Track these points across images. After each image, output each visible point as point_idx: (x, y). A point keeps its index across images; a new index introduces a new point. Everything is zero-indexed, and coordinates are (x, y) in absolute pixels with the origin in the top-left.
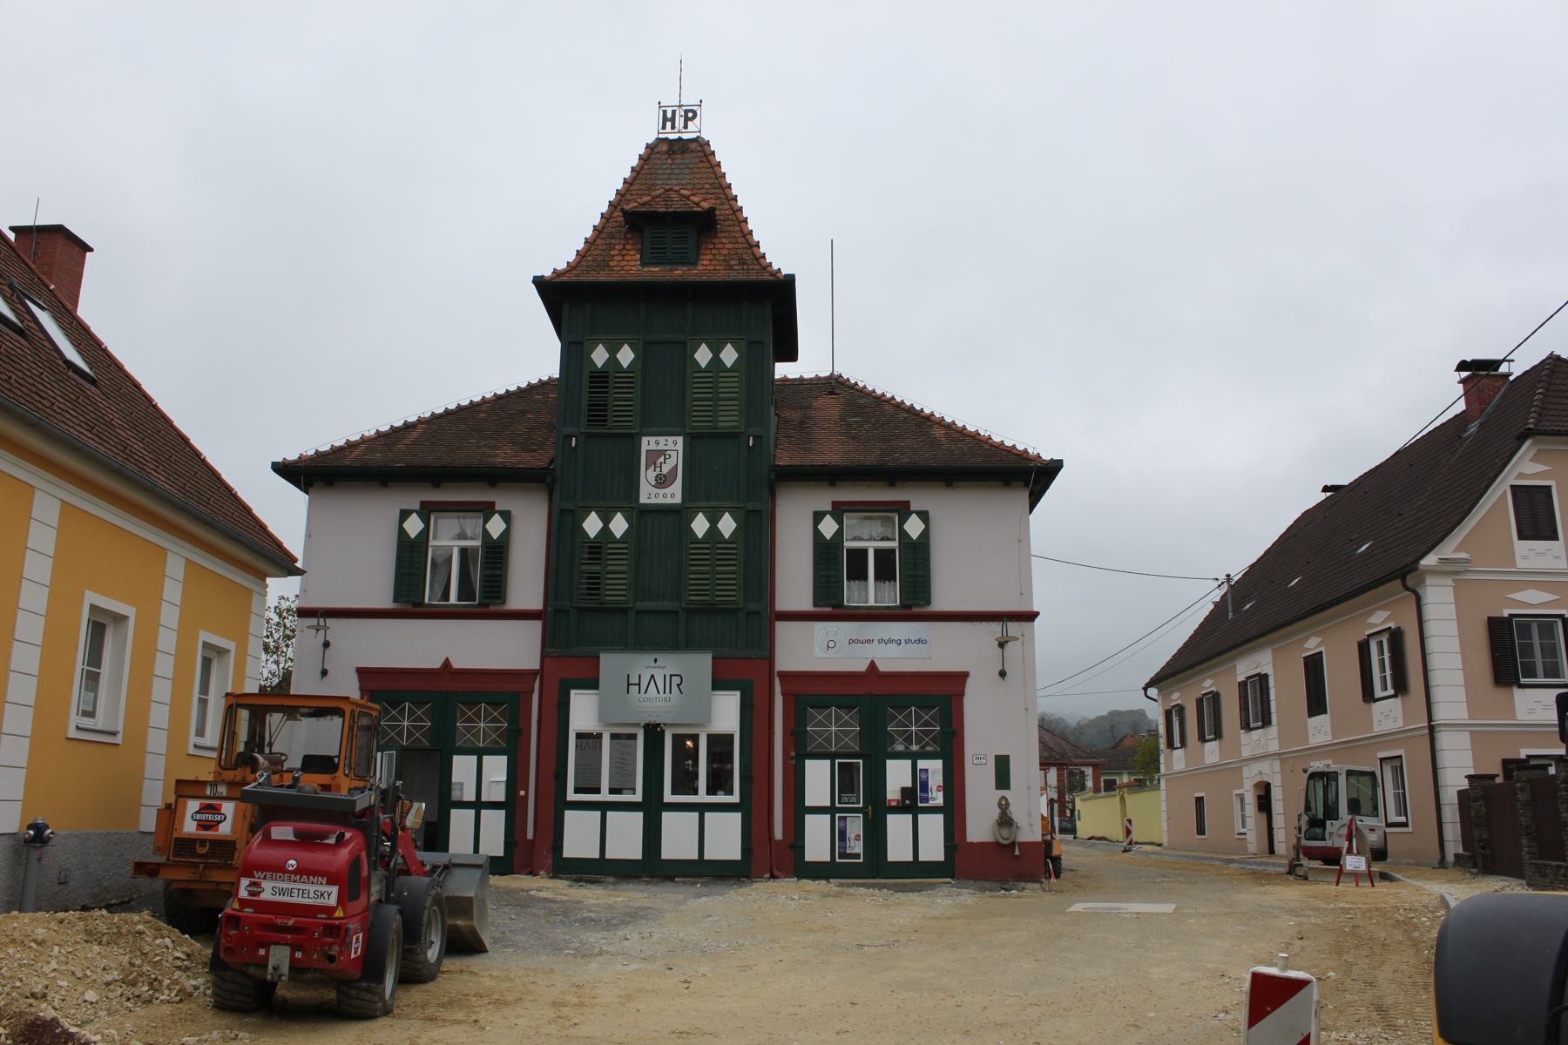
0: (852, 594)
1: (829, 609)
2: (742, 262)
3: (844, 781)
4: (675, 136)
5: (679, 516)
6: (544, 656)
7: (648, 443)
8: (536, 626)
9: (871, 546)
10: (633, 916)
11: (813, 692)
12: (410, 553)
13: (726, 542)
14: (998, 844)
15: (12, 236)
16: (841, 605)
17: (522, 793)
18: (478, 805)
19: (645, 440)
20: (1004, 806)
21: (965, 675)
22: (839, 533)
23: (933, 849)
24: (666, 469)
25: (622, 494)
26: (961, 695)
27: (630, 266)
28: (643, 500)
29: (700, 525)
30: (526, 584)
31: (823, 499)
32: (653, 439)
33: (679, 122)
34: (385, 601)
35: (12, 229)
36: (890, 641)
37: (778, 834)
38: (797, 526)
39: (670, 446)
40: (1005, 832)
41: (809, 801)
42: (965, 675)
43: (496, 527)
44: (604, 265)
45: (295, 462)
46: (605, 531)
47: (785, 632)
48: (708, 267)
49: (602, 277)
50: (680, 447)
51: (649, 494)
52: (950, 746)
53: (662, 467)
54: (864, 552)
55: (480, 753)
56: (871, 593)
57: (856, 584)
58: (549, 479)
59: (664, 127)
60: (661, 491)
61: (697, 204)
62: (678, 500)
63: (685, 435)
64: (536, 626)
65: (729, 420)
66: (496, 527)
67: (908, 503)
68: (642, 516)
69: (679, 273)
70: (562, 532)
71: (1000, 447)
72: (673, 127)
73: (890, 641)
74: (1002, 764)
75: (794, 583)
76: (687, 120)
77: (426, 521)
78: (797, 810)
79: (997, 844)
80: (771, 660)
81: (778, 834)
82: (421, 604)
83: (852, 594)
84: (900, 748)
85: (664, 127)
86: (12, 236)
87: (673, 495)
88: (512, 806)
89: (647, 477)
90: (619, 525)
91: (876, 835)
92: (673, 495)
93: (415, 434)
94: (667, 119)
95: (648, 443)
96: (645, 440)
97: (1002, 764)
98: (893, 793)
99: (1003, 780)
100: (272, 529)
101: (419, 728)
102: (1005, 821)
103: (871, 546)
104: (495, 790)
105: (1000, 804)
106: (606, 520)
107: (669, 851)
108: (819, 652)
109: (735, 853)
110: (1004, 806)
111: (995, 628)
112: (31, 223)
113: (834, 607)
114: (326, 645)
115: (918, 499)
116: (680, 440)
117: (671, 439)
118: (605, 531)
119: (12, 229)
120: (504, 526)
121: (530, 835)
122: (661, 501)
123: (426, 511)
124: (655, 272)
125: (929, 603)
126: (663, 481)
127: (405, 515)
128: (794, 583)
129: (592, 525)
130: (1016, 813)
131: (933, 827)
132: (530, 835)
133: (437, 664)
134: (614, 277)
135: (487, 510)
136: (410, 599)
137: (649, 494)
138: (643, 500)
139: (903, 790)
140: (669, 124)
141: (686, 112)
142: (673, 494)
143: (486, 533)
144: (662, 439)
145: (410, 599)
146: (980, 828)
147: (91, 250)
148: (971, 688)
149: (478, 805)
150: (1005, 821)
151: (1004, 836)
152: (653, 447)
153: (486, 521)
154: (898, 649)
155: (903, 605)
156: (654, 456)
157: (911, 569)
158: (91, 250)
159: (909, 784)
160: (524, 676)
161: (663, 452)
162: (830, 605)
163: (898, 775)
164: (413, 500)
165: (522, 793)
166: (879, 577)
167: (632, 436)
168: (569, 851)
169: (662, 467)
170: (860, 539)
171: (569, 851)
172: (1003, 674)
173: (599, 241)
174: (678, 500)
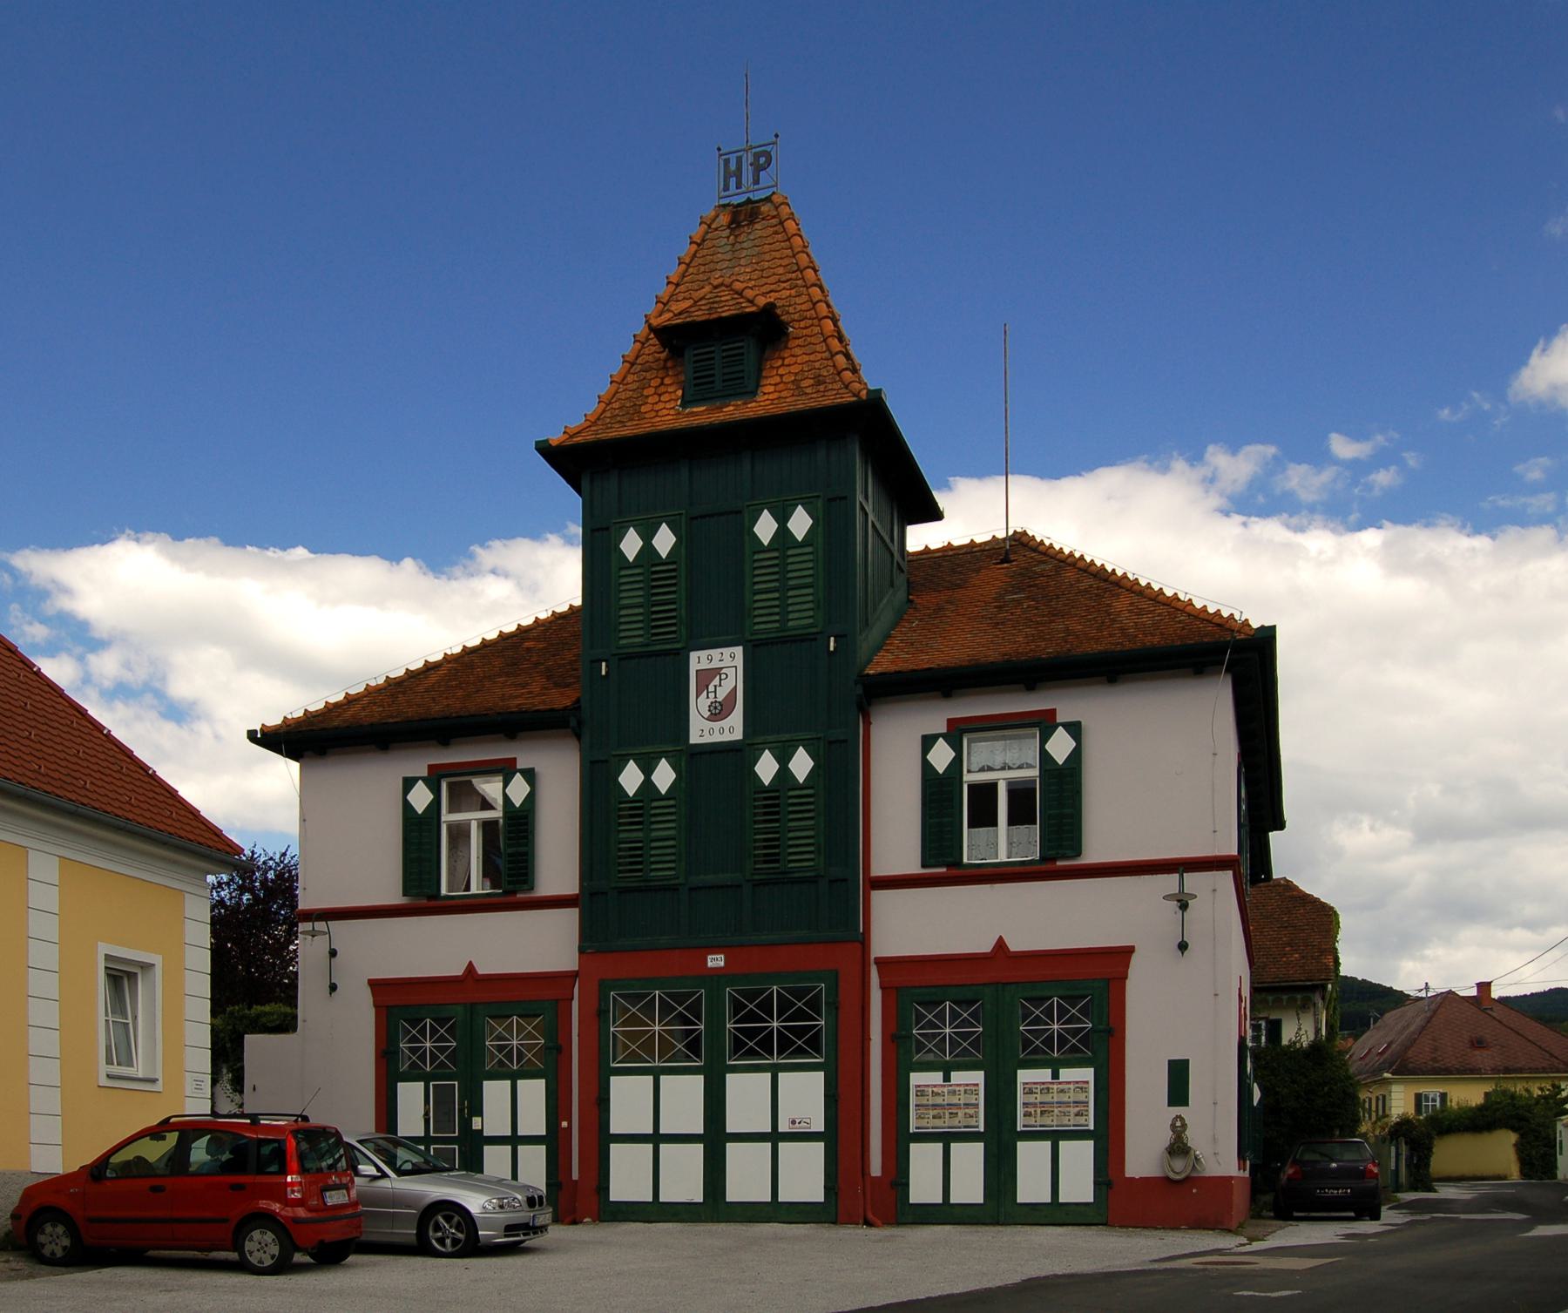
0: (975, 846)
1: (944, 870)
2: (819, 381)
3: (439, 1107)
4: (742, 199)
5: (738, 755)
7: (698, 660)
8: (571, 916)
9: (1002, 780)
10: (375, 1264)
11: (926, 983)
12: (419, 833)
13: (663, 798)
14: (1167, 1179)
16: (958, 863)
18: (514, 1140)
19: (693, 656)
20: (1179, 1128)
21: (1129, 951)
22: (957, 763)
23: (1079, 1186)
24: (722, 694)
25: (662, 729)
27: (668, 411)
28: (694, 739)
29: (766, 768)
30: (558, 863)
31: (934, 717)
32: (703, 654)
33: (747, 172)
34: (393, 895)
37: (876, 1169)
38: (899, 755)
39: (727, 662)
40: (1179, 1164)
42: (1129, 951)
43: (1060, 746)
44: (635, 412)
45: (280, 726)
46: (648, 785)
48: (774, 395)
49: (627, 431)
50: (739, 661)
51: (702, 731)
52: (1102, 1045)
53: (716, 692)
54: (993, 787)
55: (514, 1077)
56: (1003, 842)
57: (983, 831)
58: (573, 722)
59: (726, 188)
60: (716, 725)
61: (751, 302)
62: (738, 735)
64: (571, 916)
65: (801, 617)
66: (1060, 746)
67: (1053, 712)
68: (693, 760)
69: (733, 411)
71: (1202, 617)
74: (1178, 1075)
76: (758, 169)
77: (957, 747)
78: (899, 1140)
79: (1167, 1180)
80: (864, 942)
81: (876, 1169)
82: (436, 895)
83: (975, 846)
85: (726, 188)
87: (732, 729)
88: (554, 1140)
89: (699, 706)
90: (664, 776)
91: (1000, 1170)
92: (732, 729)
93: (434, 677)
94: (732, 174)
95: (698, 660)
96: (693, 656)
97: (1178, 1075)
99: (1178, 1090)
101: (442, 1050)
102: (1178, 1148)
103: (1002, 780)
104: (534, 1121)
105: (1173, 1126)
106: (648, 770)
107: (736, 1191)
109: (977, 1197)
110: (1179, 1128)
111: (1169, 882)
113: (948, 866)
114: (333, 953)
115: (1067, 705)
117: (727, 651)
118: (648, 785)
120: (431, 797)
122: (717, 738)
123: (956, 733)
124: (702, 415)
125: (1079, 854)
126: (719, 712)
127: (409, 784)
128: (895, 838)
129: (630, 778)
130: (1193, 1137)
131: (1079, 1158)
132: (575, 1176)
133: (458, 971)
134: (645, 428)
135: (1045, 723)
136: (423, 894)
137: (702, 731)
138: (694, 739)
140: (733, 181)
141: (757, 156)
142: (732, 728)
143: (1045, 757)
144: (715, 653)
145: (423, 894)
146: (1143, 1156)
149: (514, 1140)
150: (1178, 1148)
151: (1179, 1166)
152: (705, 665)
153: (1044, 740)
155: (1043, 859)
156: (706, 677)
157: (1055, 804)
160: (570, 977)
161: (717, 671)
162: (943, 863)
164: (418, 766)
165: (564, 1124)
166: (1013, 821)
167: (676, 652)
169: (716, 692)
170: (990, 769)
171: (916, 1196)
172: (1183, 946)
173: (630, 378)
174: (738, 735)
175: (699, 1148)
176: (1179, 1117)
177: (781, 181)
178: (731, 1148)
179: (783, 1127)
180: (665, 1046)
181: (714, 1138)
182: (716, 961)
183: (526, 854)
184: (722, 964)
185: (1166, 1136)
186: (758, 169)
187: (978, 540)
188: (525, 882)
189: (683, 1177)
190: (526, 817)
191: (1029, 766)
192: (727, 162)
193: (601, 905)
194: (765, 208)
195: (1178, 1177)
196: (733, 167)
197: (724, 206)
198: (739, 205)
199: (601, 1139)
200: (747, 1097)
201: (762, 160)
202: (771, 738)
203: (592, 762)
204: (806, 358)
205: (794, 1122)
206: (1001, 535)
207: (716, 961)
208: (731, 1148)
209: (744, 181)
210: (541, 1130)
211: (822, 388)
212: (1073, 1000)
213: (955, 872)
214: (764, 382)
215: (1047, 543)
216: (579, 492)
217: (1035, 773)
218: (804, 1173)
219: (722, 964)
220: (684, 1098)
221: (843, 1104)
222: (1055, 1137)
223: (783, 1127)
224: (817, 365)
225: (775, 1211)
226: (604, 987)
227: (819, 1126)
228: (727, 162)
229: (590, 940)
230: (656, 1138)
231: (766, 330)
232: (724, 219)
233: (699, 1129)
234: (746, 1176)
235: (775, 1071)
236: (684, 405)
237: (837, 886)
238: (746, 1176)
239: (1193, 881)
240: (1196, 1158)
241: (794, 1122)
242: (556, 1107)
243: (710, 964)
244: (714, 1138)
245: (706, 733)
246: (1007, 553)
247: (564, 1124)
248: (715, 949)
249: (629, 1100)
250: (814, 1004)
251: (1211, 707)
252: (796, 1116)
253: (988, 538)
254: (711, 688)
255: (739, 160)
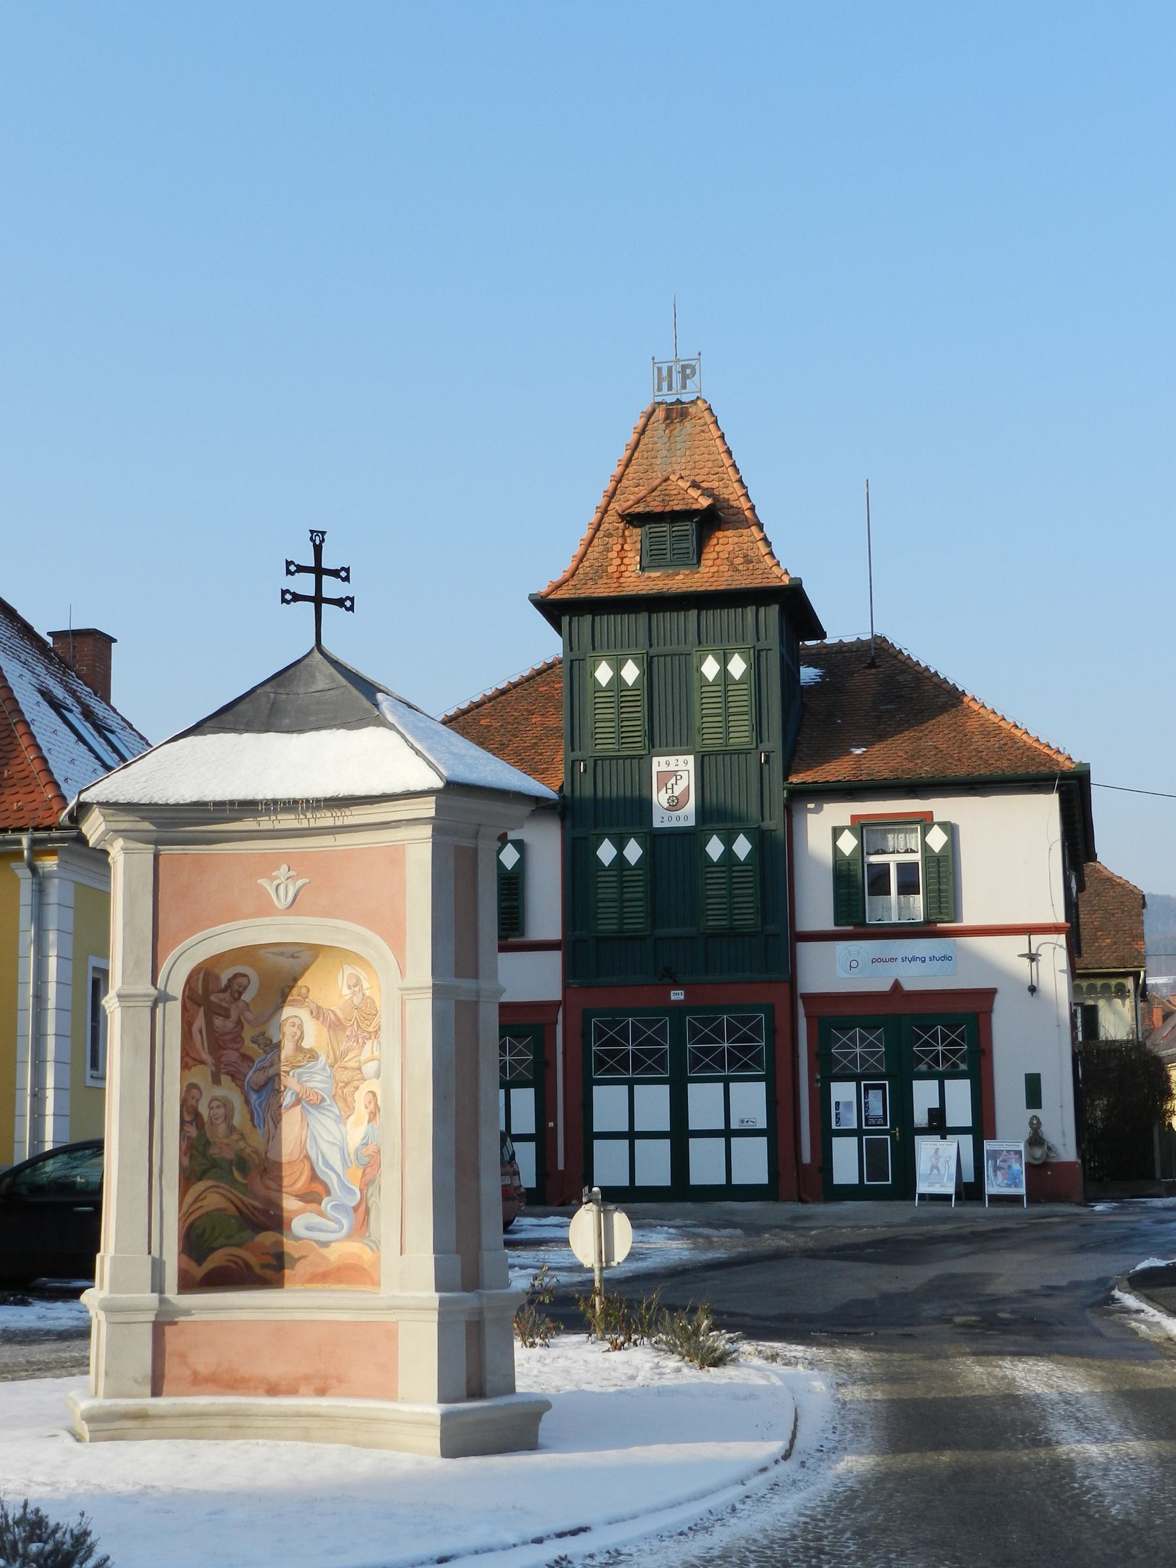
1: (850, 928)
4: (671, 399)
5: (690, 839)
6: (565, 987)
7: (659, 764)
11: (840, 1013)
15: (50, 640)
16: (863, 923)
17: (551, 1124)
19: (655, 760)
20: (1035, 1125)
26: (989, 1012)
28: (657, 824)
29: (715, 848)
30: (545, 914)
32: (663, 759)
35: (49, 634)
36: (914, 959)
37: (806, 1157)
39: (681, 766)
40: (1038, 1152)
41: (532, 1145)
47: (808, 953)
48: (716, 568)
51: (660, 820)
52: (978, 1070)
59: (660, 389)
62: (691, 822)
63: (696, 753)
66: (937, 839)
70: (577, 860)
72: (670, 388)
73: (914, 959)
74: (1033, 1084)
75: (816, 906)
76: (685, 377)
78: (825, 1135)
80: (792, 981)
81: (806, 1157)
84: (923, 1067)
85: (660, 389)
86: (50, 640)
88: (542, 1137)
90: (633, 852)
94: (663, 378)
95: (659, 764)
96: (655, 760)
97: (1033, 1084)
98: (920, 1118)
99: (1034, 1096)
100: (342, 732)
103: (892, 860)
105: (1031, 1123)
108: (841, 973)
110: (1035, 1125)
112: (67, 628)
113: (855, 925)
115: (942, 808)
116: (691, 759)
117: (681, 758)
119: (49, 634)
121: (561, 1167)
122: (674, 824)
129: (606, 852)
132: (561, 1167)
135: (925, 821)
139: (931, 1111)
140: (665, 385)
141: (684, 368)
143: (926, 847)
144: (672, 759)
147: (115, 641)
148: (999, 1004)
150: (1036, 1140)
152: (664, 768)
153: (924, 834)
154: (916, 968)
156: (666, 776)
158: (115, 641)
159: (936, 1105)
163: (924, 1094)
167: (641, 757)
168: (837, 1180)
171: (837, 1180)
174: (691, 822)
175: (667, 1143)
176: (1035, 1117)
177: (708, 386)
178: (693, 1143)
179: (734, 1125)
180: (638, 1063)
181: (680, 1134)
182: (677, 995)
183: (517, 907)
184: (682, 997)
185: (1027, 1132)
186: (685, 377)
187: (846, 640)
188: (517, 929)
189: (655, 1167)
190: (516, 878)
191: (912, 851)
192: (660, 369)
193: (580, 949)
194: (692, 410)
195: (1037, 1163)
196: (665, 373)
197: (659, 403)
198: (671, 404)
199: (584, 1135)
200: (705, 1102)
201: (688, 371)
202: (720, 826)
203: (574, 839)
204: (736, 540)
205: (742, 1121)
206: (867, 637)
207: (677, 995)
208: (693, 1143)
209: (674, 385)
210: (531, 1129)
211: (751, 566)
212: (952, 1028)
213: (861, 930)
214: (706, 550)
215: (906, 653)
216: (560, 634)
217: (917, 857)
218: (752, 1163)
219: (682, 997)
220: (653, 1104)
221: (780, 1105)
222: (665, 656)
223: (734, 1125)
224: (745, 546)
225: (730, 1191)
226: (587, 1015)
227: (762, 1124)
228: (660, 369)
229: (570, 971)
230: (632, 1135)
231: (712, 519)
232: (660, 414)
233: (667, 1127)
234: (706, 1164)
235: (726, 1081)
236: (642, 569)
237: (773, 938)
238: (706, 1164)
239: (1037, 939)
240: (1049, 1148)
241: (742, 1121)
242: (543, 1110)
243: (673, 998)
244: (680, 1134)
245: (666, 819)
246: (873, 659)
247: (551, 1124)
248: (677, 985)
249: (609, 1104)
250: (756, 1029)
251: (1045, 808)
252: (745, 1117)
253: (853, 639)
254: (669, 786)
255: (670, 369)
